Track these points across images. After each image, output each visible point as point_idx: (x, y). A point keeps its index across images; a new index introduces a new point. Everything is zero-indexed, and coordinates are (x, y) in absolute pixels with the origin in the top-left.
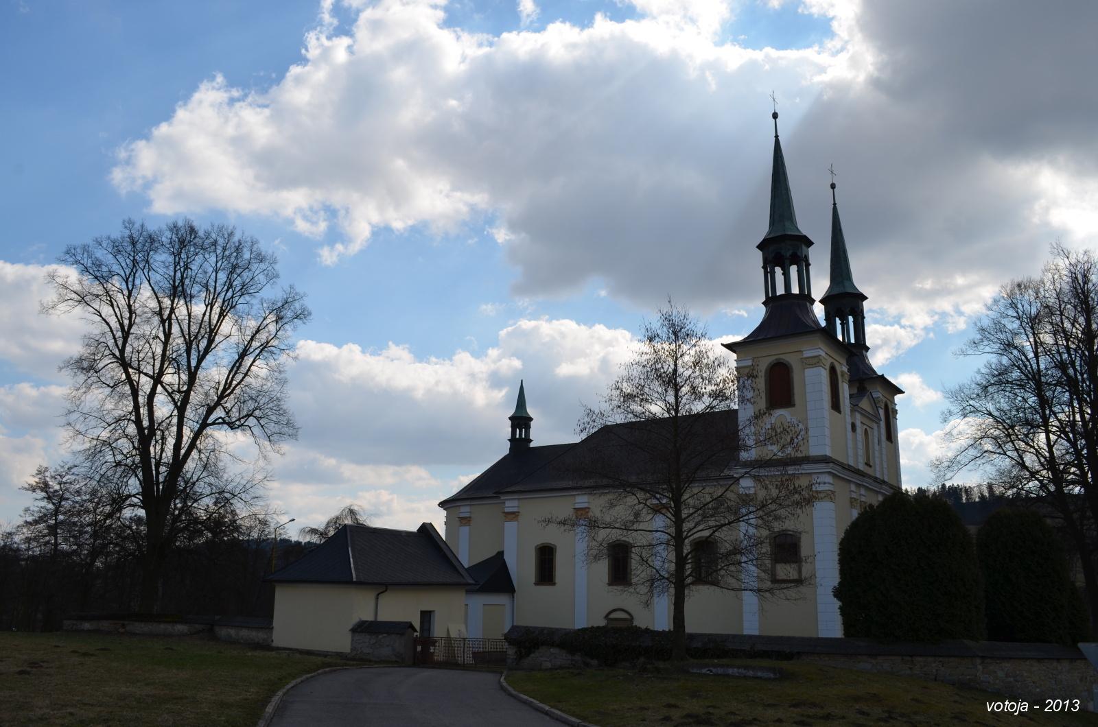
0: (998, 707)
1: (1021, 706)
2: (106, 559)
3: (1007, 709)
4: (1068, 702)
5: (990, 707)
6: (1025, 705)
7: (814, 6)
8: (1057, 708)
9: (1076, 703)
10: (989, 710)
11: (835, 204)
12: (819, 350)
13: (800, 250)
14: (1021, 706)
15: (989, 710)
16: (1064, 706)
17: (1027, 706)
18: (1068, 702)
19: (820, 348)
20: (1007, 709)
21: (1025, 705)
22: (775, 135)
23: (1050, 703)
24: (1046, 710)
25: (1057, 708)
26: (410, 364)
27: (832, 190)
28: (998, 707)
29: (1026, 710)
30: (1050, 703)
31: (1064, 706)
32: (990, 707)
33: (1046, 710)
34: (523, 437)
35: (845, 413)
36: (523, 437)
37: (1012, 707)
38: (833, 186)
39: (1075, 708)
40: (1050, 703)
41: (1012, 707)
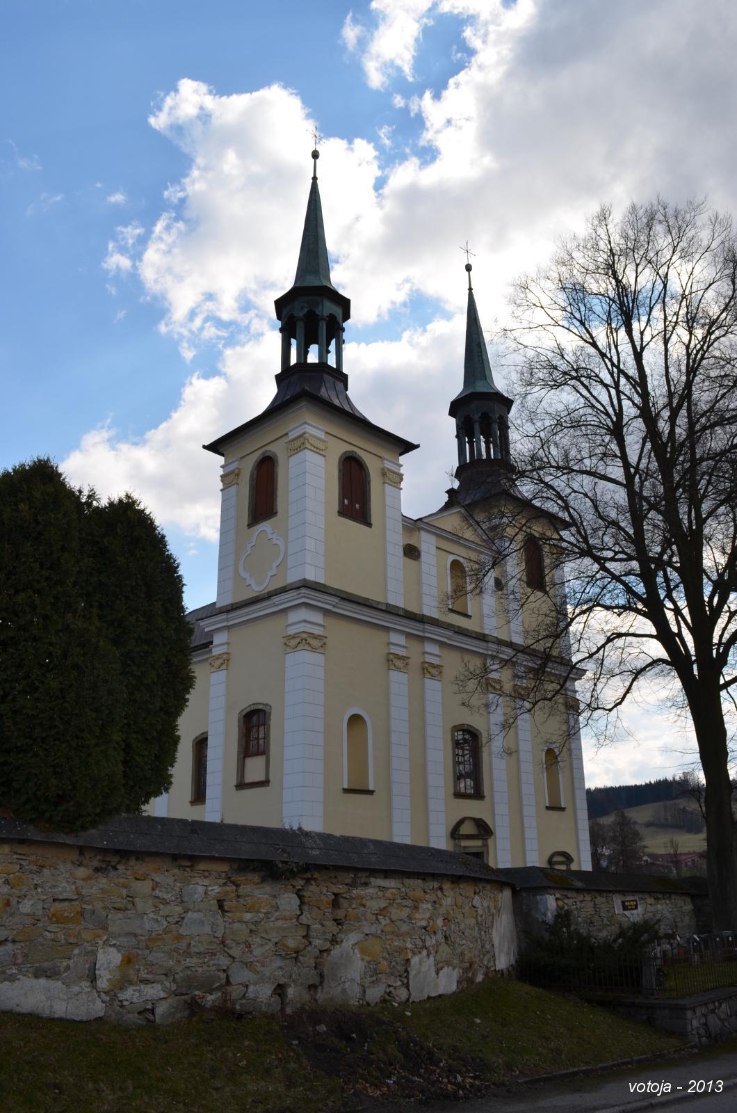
0: (641, 1088)
1: (664, 1087)
2: (516, 479)
3: (650, 1090)
4: (711, 1082)
5: (632, 1087)
6: (668, 1086)
7: (175, 95)
8: (700, 1089)
9: (720, 1083)
10: (632, 1091)
11: (470, 289)
12: (306, 426)
13: (320, 306)
14: (664, 1087)
15: (632, 1091)
16: (707, 1086)
17: (670, 1087)
18: (711, 1082)
19: (305, 423)
20: (650, 1090)
21: (668, 1086)
22: (312, 176)
23: (693, 1084)
24: (689, 1091)
25: (700, 1089)
26: (204, 94)
27: (467, 273)
28: (641, 1088)
29: (669, 1091)
30: (693, 1083)
31: (707, 1086)
32: (632, 1087)
33: (689, 1091)
34: (492, 457)
35: (384, 528)
36: (492, 457)
37: (655, 1088)
38: (469, 268)
39: (719, 1089)
40: (693, 1084)
41: (655, 1088)
